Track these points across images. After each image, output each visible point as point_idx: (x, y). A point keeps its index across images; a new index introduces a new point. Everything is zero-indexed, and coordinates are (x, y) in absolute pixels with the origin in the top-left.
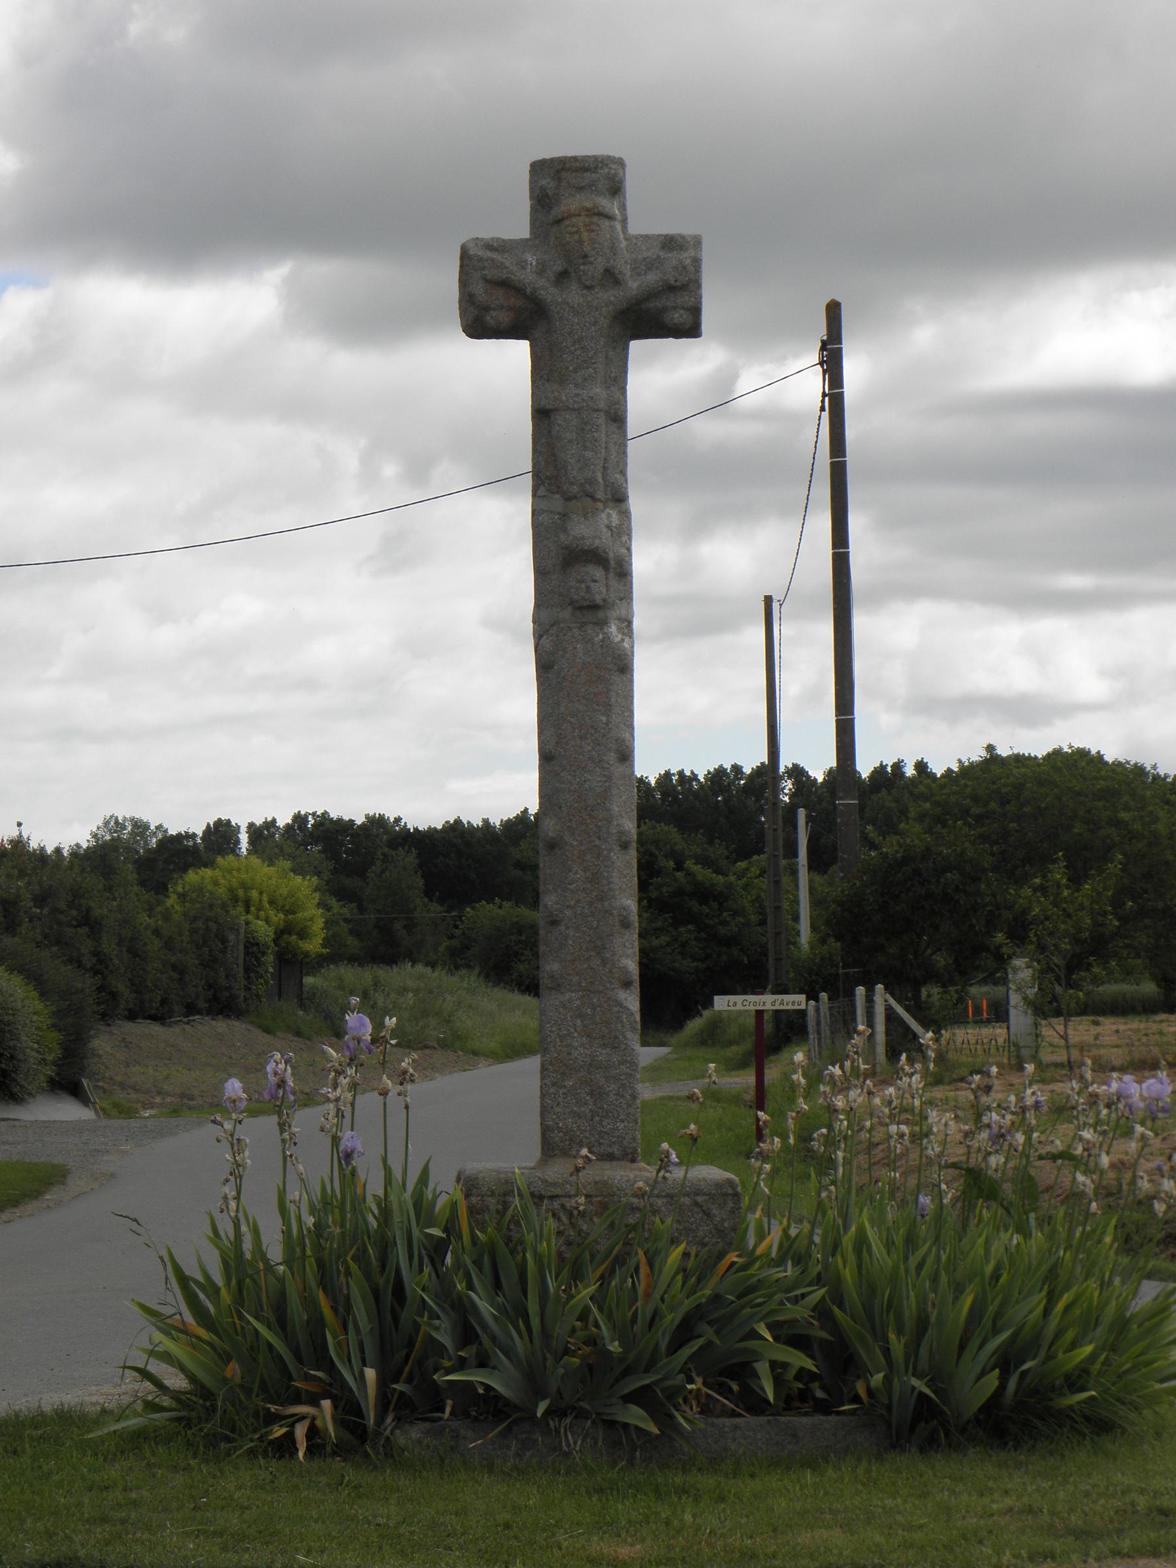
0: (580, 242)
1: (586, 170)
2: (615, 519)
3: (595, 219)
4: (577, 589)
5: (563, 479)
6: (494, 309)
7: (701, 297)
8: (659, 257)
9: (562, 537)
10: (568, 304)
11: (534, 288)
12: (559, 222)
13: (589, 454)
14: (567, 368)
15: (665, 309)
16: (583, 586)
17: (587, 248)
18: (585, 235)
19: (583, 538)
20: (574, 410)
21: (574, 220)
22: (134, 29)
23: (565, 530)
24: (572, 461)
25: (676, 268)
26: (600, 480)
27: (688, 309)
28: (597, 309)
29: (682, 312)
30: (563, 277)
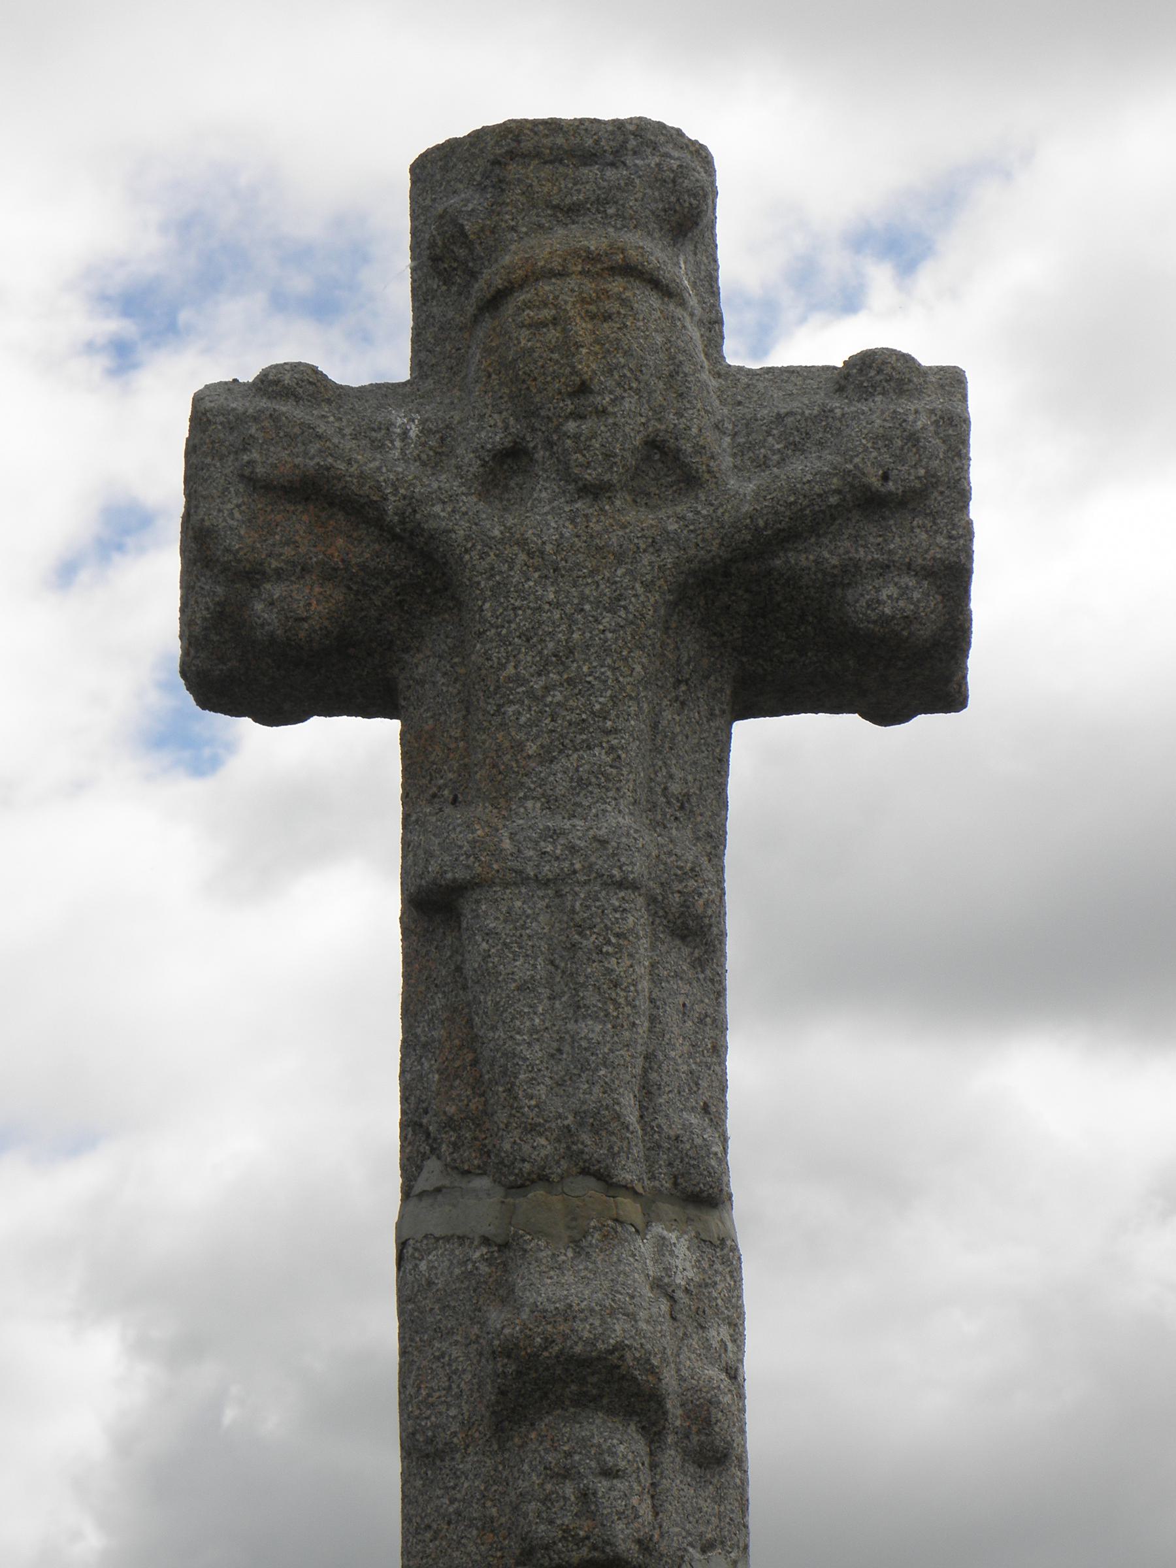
0: (568, 347)
1: (588, 157)
2: (684, 1263)
3: (616, 285)
4: (546, 1500)
5: (502, 1117)
6: (279, 575)
7: (967, 532)
8: (826, 412)
9: (496, 1317)
10: (523, 543)
11: (409, 498)
12: (495, 301)
13: (590, 1029)
14: (519, 747)
15: (850, 573)
16: (569, 1489)
17: (587, 364)
18: (582, 329)
19: (568, 1314)
20: (546, 883)
21: (546, 288)
22: (230, 1415)
23: (506, 1295)
24: (535, 1054)
25: (885, 439)
26: (632, 1119)
27: (928, 573)
28: (620, 559)
29: (909, 581)
30: (507, 465)
